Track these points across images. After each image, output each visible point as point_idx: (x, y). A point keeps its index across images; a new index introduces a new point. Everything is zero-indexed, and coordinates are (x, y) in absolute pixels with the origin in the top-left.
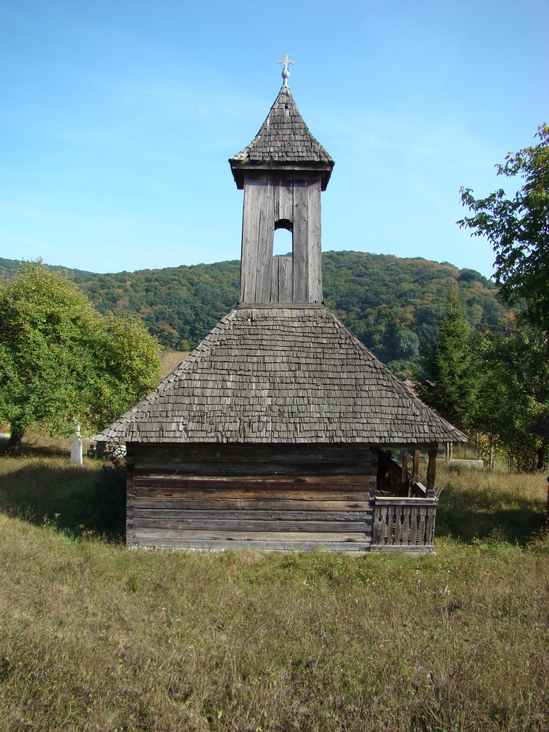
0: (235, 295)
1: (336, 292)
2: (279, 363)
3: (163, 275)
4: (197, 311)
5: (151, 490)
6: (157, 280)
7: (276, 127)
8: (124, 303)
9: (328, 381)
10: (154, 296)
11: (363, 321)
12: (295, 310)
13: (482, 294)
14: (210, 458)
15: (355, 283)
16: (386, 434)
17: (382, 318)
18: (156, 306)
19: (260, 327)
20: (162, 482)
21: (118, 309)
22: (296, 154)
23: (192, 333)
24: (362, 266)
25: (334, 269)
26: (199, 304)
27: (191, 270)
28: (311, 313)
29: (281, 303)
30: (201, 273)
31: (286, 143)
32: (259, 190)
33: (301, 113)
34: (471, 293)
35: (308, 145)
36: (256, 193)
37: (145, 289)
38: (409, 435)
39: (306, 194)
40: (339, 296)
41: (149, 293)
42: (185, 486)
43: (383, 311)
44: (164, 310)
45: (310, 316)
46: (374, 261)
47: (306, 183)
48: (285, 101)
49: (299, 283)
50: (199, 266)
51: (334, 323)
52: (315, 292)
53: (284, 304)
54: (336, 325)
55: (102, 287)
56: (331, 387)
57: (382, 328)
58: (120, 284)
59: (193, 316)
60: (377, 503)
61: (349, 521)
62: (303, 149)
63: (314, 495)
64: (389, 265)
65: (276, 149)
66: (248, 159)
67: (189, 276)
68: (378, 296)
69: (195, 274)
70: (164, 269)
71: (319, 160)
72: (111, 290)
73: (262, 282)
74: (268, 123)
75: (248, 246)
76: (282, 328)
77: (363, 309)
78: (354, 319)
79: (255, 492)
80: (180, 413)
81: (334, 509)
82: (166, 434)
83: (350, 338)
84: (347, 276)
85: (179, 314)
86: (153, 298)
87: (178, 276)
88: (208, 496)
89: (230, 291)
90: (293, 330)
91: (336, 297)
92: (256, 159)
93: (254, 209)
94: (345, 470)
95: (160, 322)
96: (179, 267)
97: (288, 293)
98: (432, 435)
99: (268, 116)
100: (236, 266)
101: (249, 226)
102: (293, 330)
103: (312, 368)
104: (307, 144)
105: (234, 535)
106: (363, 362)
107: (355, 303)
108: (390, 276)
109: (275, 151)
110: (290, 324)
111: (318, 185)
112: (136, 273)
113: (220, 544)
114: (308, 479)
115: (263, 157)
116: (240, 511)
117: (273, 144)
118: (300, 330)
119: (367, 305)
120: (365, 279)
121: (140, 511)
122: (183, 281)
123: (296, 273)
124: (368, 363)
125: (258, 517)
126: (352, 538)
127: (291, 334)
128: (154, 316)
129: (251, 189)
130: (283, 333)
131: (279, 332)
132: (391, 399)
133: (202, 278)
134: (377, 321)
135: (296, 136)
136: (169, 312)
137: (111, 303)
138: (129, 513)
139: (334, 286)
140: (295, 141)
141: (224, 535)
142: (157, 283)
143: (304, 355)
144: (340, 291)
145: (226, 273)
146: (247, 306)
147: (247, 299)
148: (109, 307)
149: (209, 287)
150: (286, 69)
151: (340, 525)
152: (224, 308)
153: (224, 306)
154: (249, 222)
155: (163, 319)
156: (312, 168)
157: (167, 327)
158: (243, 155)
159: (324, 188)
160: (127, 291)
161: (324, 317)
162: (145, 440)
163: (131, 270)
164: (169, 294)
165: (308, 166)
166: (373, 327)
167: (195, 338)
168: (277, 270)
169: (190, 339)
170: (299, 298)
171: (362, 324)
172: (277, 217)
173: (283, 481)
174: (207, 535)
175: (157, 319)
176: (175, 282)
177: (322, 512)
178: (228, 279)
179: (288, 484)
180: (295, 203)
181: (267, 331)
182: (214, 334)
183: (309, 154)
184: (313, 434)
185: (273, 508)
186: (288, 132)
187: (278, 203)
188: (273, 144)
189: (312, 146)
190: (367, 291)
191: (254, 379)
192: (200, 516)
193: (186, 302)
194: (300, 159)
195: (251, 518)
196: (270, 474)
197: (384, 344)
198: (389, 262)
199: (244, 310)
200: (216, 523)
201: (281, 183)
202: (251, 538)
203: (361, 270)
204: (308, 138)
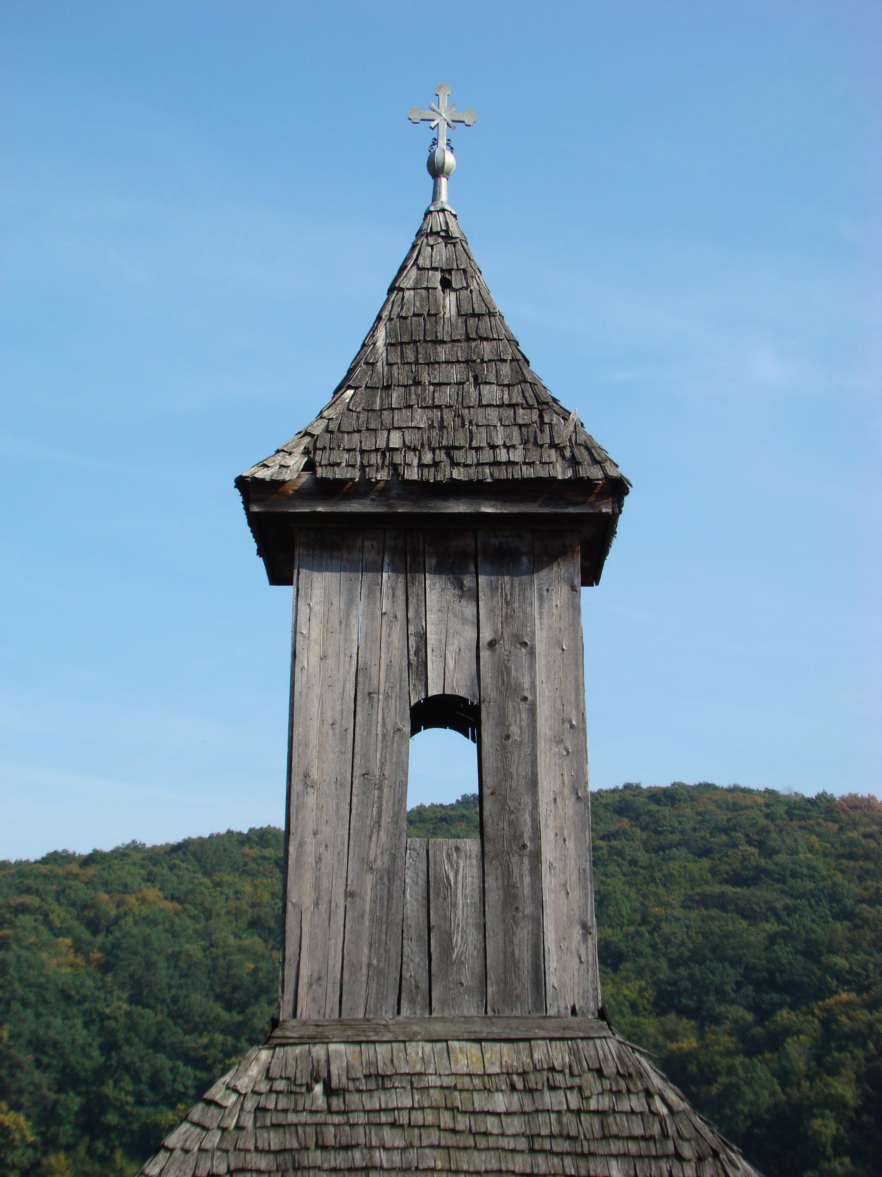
0: (263, 964)
1: (654, 947)
4: (113, 1032)
7: (410, 356)
11: (765, 1062)
12: (497, 1046)
15: (723, 908)
17: (840, 1049)
19: (362, 1118)
22: (487, 456)
23: (91, 1123)
24: (750, 842)
25: (643, 857)
26: (119, 1005)
27: (91, 871)
28: (559, 1055)
29: (442, 1019)
30: (129, 879)
31: (448, 416)
32: (351, 591)
33: (500, 303)
35: (527, 421)
36: (339, 603)
39: (523, 599)
40: (664, 963)
43: (844, 1019)
45: (552, 1069)
46: (795, 823)
47: (525, 559)
48: (439, 262)
50: (123, 854)
51: (648, 1094)
52: (570, 970)
53: (452, 1021)
54: (658, 1104)
57: (844, 1088)
59: (96, 1053)
62: (510, 436)
64: (854, 834)
65: (411, 438)
66: (306, 476)
67: (82, 893)
68: (817, 961)
69: (106, 884)
71: (569, 474)
73: (366, 935)
74: (380, 343)
75: (311, 800)
76: (446, 1119)
77: (763, 1013)
78: (729, 1053)
83: (716, 1154)
84: (692, 880)
85: (38, 1045)
87: (37, 893)
89: (243, 950)
90: (491, 1124)
91: (652, 962)
92: (339, 474)
93: (331, 662)
96: (44, 861)
97: (468, 976)
99: (379, 318)
100: (267, 852)
101: (315, 723)
102: (491, 1124)
104: (523, 416)
107: (728, 989)
108: (861, 878)
109: (405, 443)
110: (479, 1101)
111: (572, 567)
115: (363, 467)
117: (399, 418)
118: (516, 1125)
119: (775, 996)
120: (765, 894)
122: (59, 914)
123: (494, 897)
127: (482, 1142)
129: (321, 585)
130: (450, 1140)
131: (434, 1137)
133: (131, 900)
134: (822, 1062)
135: (485, 390)
139: (644, 922)
140: (481, 406)
144: (667, 942)
145: (229, 878)
146: (310, 1031)
147: (310, 1003)
150: (442, 143)
152: (217, 1018)
153: (218, 1009)
154: (315, 709)
156: (542, 505)
158: (291, 461)
159: (591, 576)
161: (610, 1069)
165: (533, 499)
166: (805, 1084)
167: (100, 1145)
168: (421, 890)
169: (82, 1150)
170: (509, 997)
171: (762, 1072)
172: (421, 688)
176: (25, 920)
178: (232, 904)
180: (487, 635)
181: (387, 1132)
182: (178, 1153)
183: (534, 455)
186: (455, 373)
187: (423, 637)
188: (399, 418)
189: (542, 423)
190: (772, 939)
194: (502, 474)
197: (856, 1155)
198: (855, 824)
199: (298, 1049)
201: (431, 562)
203: (745, 858)
204: (529, 394)
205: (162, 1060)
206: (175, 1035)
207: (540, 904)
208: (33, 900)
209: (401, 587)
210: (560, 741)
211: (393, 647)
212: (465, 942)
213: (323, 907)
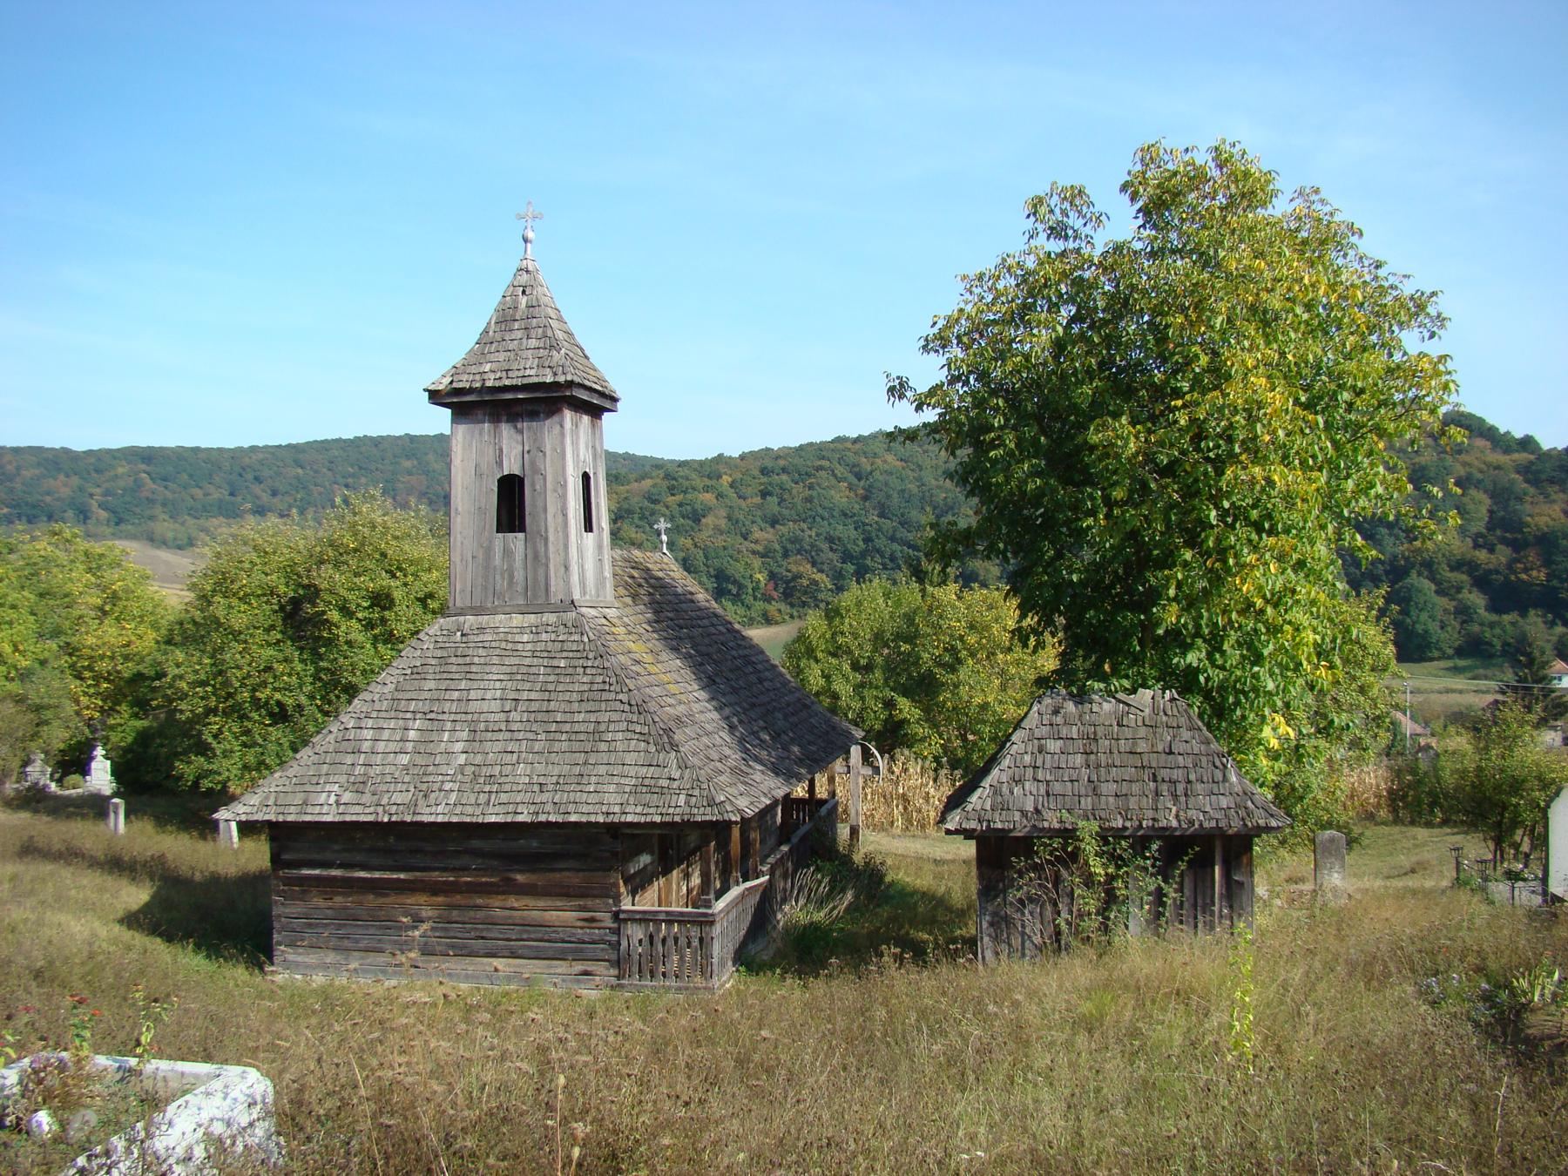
2: (488, 697)
5: (304, 892)
6: (784, 470)
9: (553, 727)
13: (1489, 465)
14: (381, 844)
16: (617, 809)
20: (317, 878)
21: (704, 535)
26: (873, 517)
27: (857, 446)
34: (1465, 464)
38: (652, 810)
42: (349, 885)
44: (798, 533)
48: (525, 283)
49: (535, 571)
55: (672, 490)
56: (558, 736)
60: (622, 916)
61: (584, 942)
63: (531, 902)
67: (851, 458)
72: (689, 496)
80: (336, 778)
82: (310, 809)
85: (830, 539)
86: (777, 509)
88: (381, 900)
90: (520, 647)
94: (572, 863)
95: (791, 560)
96: (832, 442)
97: (520, 588)
98: (687, 810)
102: (520, 647)
103: (535, 706)
106: (612, 696)
110: (517, 638)
112: (743, 457)
114: (520, 878)
122: (840, 470)
124: (620, 696)
128: (777, 547)
131: (498, 652)
133: (878, 461)
138: (276, 925)
142: (784, 477)
143: (527, 686)
149: (894, 482)
155: (799, 552)
157: (806, 569)
162: (281, 819)
163: (734, 452)
164: (809, 500)
174: (382, 959)
175: (786, 555)
176: (822, 473)
179: (492, 884)
184: (511, 808)
186: (519, 334)
191: (449, 725)
193: (845, 515)
194: (526, 381)
196: (465, 869)
205: (895, 546)
206: (902, 533)
207: (547, 558)
208: (826, 463)
212: (519, 575)
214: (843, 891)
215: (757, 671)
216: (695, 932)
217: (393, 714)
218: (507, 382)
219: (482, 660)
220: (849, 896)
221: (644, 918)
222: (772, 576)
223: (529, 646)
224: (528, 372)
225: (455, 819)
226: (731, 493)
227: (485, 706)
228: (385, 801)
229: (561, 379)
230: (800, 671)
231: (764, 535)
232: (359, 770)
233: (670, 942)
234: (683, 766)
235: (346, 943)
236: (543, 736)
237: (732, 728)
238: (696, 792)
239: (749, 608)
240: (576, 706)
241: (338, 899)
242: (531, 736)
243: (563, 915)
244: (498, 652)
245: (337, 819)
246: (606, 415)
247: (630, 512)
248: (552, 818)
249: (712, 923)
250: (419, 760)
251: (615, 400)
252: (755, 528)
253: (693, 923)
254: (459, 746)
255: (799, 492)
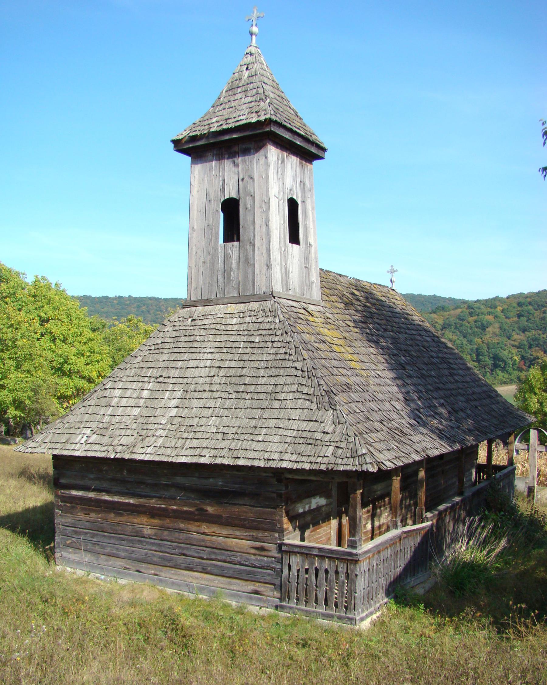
2: (202, 364)
3: (536, 299)
5: (73, 508)
6: (530, 304)
8: (495, 330)
9: (242, 388)
10: (527, 321)
16: (276, 456)
18: (529, 332)
21: (488, 337)
37: (518, 314)
41: (521, 318)
44: (537, 336)
47: (252, 151)
55: (471, 314)
56: (244, 396)
58: (490, 310)
60: (284, 548)
61: (255, 567)
70: (539, 292)
72: (480, 317)
79: (160, 520)
81: (239, 550)
82: (68, 446)
86: (526, 323)
88: (118, 519)
95: (533, 350)
97: (234, 284)
102: (229, 327)
103: (231, 372)
105: (143, 567)
106: (290, 364)
110: (229, 321)
112: (508, 298)
113: (130, 574)
116: (148, 540)
121: (66, 529)
124: (297, 364)
125: (163, 549)
126: (259, 589)
128: (526, 343)
131: (213, 332)
132: (306, 411)
136: (543, 338)
137: (480, 330)
141: (133, 566)
142: (530, 307)
143: (230, 356)
148: (478, 335)
151: (246, 570)
155: (537, 346)
160: (497, 317)
163: (504, 294)
168: (223, 259)
173: (185, 509)
174: (119, 563)
175: (530, 347)
177: (226, 552)
180: (241, 177)
184: (198, 452)
185: (177, 540)
187: (224, 180)
192: (112, 541)
195: (157, 549)
200: (127, 550)
201: (226, 156)
202: (158, 573)
207: (255, 260)
209: (218, 168)
210: (261, 207)
211: (216, 184)
213: (197, 267)
214: (499, 538)
215: (450, 368)
216: (342, 568)
217: (136, 378)
218: (225, 127)
219: (202, 339)
220: (503, 543)
221: (305, 553)
222: (523, 358)
223: (236, 327)
224: (241, 118)
225: (157, 459)
226: (502, 316)
227: (197, 372)
228: (115, 442)
229: (262, 118)
230: (525, 400)
231: (519, 337)
232: (106, 419)
233: (322, 574)
234: (337, 422)
235: (97, 548)
236: (233, 396)
237: (407, 400)
238: (343, 445)
239: (510, 374)
240: (262, 372)
241: (93, 515)
242: (224, 395)
243: (240, 543)
244: (213, 332)
245: (82, 455)
246: (315, 162)
247: (449, 325)
248: (226, 462)
249: (356, 562)
250: (146, 412)
251: (324, 150)
252: (514, 333)
253: (341, 560)
254: (174, 403)
255: (538, 314)
